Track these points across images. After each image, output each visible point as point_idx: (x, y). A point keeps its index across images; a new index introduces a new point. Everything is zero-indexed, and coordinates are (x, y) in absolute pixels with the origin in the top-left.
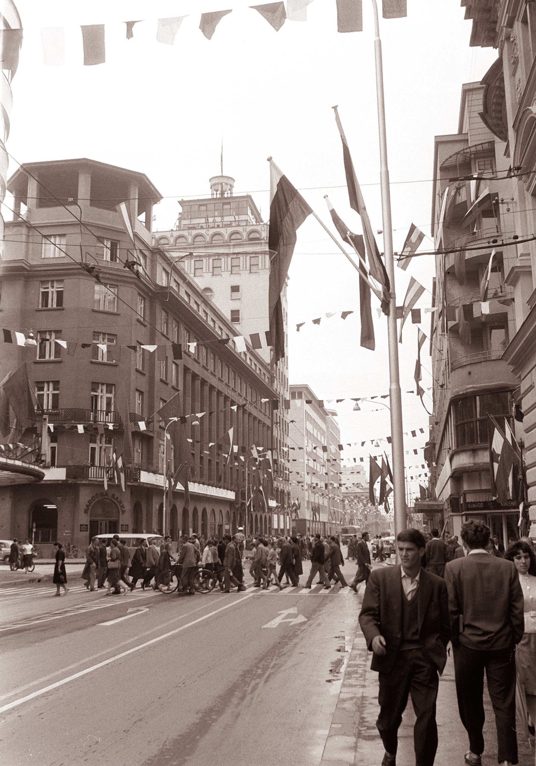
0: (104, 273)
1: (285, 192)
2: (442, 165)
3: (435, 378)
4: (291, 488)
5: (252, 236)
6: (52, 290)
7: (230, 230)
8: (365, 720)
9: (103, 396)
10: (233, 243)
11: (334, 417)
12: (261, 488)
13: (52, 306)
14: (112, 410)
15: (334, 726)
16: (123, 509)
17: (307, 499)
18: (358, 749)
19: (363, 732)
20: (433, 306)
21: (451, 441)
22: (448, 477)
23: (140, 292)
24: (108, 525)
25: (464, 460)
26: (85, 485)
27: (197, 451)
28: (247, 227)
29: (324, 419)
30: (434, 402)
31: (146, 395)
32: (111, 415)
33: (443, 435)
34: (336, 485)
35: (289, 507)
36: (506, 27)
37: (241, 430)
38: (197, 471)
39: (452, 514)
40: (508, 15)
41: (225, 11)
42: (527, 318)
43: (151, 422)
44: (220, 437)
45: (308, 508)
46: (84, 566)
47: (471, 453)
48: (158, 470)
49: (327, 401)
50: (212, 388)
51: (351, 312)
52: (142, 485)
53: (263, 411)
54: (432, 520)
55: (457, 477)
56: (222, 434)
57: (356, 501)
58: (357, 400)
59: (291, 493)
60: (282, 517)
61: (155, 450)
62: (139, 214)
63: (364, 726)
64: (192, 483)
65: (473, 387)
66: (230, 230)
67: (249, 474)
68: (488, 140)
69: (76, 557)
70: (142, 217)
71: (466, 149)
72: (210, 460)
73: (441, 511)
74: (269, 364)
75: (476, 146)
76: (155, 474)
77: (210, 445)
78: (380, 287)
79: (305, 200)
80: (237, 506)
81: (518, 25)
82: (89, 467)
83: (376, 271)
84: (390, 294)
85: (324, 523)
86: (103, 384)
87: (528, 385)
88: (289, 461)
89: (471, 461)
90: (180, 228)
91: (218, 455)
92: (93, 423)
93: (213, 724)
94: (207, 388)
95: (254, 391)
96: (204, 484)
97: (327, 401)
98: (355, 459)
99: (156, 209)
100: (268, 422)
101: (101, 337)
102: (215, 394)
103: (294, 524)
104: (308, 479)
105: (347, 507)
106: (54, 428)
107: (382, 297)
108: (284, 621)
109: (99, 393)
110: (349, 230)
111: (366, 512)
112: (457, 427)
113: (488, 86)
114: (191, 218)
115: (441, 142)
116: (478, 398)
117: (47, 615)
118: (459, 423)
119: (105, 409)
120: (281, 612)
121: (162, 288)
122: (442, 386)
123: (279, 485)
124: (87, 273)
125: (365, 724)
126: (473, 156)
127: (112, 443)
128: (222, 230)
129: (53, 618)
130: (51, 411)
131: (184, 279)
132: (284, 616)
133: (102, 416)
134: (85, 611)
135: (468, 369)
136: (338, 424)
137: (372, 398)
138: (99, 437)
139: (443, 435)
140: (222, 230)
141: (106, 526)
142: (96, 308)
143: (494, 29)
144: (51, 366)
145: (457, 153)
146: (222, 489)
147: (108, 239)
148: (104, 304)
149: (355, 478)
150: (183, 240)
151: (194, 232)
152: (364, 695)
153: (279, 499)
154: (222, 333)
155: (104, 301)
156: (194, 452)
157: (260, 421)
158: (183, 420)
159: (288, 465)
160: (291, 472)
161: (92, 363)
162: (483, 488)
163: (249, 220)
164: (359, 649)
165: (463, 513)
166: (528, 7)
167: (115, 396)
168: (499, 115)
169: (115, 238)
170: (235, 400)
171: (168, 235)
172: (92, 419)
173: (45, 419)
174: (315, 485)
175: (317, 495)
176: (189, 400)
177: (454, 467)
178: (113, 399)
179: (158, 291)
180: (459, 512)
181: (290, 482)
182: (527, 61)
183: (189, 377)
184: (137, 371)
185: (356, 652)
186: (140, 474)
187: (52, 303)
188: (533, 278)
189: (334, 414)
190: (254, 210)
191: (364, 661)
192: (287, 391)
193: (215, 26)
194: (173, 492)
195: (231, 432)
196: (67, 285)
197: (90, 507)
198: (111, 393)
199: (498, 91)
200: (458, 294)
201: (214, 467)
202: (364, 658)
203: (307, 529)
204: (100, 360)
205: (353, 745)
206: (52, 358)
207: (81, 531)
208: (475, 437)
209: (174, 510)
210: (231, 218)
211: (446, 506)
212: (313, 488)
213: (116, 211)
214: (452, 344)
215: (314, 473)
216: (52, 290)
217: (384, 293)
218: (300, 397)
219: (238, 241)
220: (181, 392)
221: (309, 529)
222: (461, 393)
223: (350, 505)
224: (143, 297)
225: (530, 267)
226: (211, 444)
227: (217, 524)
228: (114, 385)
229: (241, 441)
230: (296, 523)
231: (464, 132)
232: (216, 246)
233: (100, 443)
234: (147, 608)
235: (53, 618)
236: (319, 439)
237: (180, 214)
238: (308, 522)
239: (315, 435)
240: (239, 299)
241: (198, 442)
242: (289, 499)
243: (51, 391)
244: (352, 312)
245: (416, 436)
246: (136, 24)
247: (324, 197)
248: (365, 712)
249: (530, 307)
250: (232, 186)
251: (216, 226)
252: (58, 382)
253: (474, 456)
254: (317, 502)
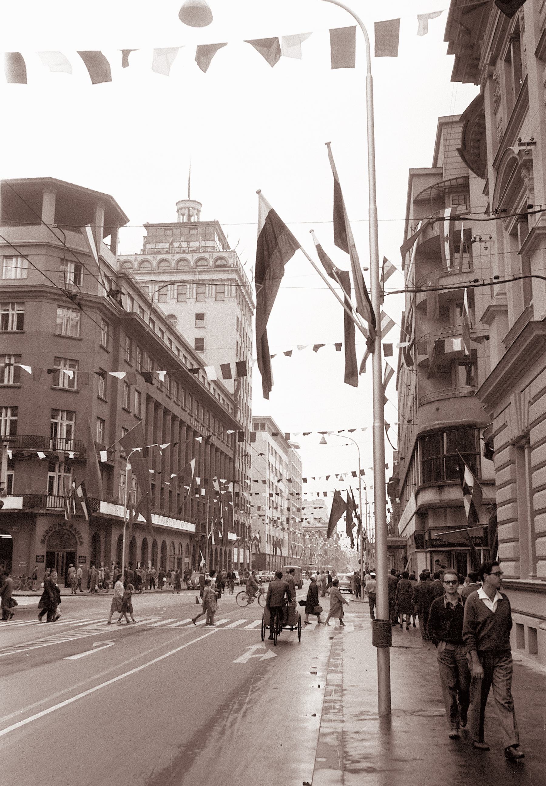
0: (86, 300)
1: (274, 225)
2: (416, 198)
3: (401, 413)
4: (252, 521)
5: (218, 263)
6: (13, 313)
7: (196, 256)
8: (349, 754)
9: (63, 423)
10: (199, 269)
11: (296, 449)
12: (222, 521)
13: (12, 329)
14: (73, 438)
15: (319, 759)
16: (81, 540)
17: (267, 532)
18: (345, 782)
19: (348, 765)
21: (416, 476)
22: (413, 513)
23: (104, 317)
24: (65, 556)
25: (429, 496)
26: (41, 515)
27: (158, 483)
28: (214, 254)
29: (286, 452)
30: (399, 436)
31: (107, 424)
32: (71, 443)
33: (409, 470)
34: (298, 520)
35: (249, 540)
36: (489, 65)
37: (202, 460)
38: (158, 502)
39: (416, 550)
40: (491, 53)
41: (220, 44)
42: (504, 357)
43: (113, 452)
44: (182, 468)
45: (268, 542)
46: (40, 598)
47: (437, 489)
48: (118, 501)
49: (294, 434)
50: (174, 417)
51: (322, 345)
52: (101, 515)
54: (394, 556)
55: (422, 513)
56: (183, 466)
57: (317, 535)
58: (323, 433)
59: (252, 526)
60: (242, 551)
61: (115, 480)
62: (105, 236)
63: (349, 760)
64: (157, 516)
65: (441, 424)
66: (196, 256)
67: (209, 506)
68: (462, 176)
69: (31, 588)
70: (108, 240)
71: (441, 183)
72: (171, 492)
73: (404, 547)
74: (232, 395)
75: (450, 180)
76: (115, 504)
77: (172, 477)
78: (366, 324)
79: (294, 235)
80: (197, 539)
81: (501, 64)
82: (46, 496)
83: (364, 309)
84: (375, 332)
85: (285, 557)
86: (63, 411)
87: (501, 424)
88: (251, 494)
89: (437, 497)
90: (144, 252)
91: (180, 486)
92: (52, 450)
93: (196, 758)
94: (169, 418)
95: (217, 423)
96: (164, 515)
97: (294, 434)
98: (318, 494)
99: (122, 232)
100: (230, 454)
101: (62, 362)
102: (177, 424)
103: (254, 558)
104: (269, 513)
105: (308, 541)
106: (13, 455)
107: (368, 334)
108: (253, 656)
109: (58, 420)
110: (334, 266)
111: (326, 547)
112: (423, 463)
113: (468, 122)
114: (156, 243)
115: (415, 175)
116: (445, 434)
117: (10, 648)
118: (426, 459)
119: (65, 437)
120: (250, 647)
121: (127, 314)
122: (409, 422)
123: (239, 518)
124: (68, 299)
125: (348, 758)
126: (447, 190)
127: (72, 472)
128: (188, 256)
129: (17, 651)
130: (8, 437)
131: (149, 305)
132: (252, 651)
133: (61, 444)
134: (50, 644)
135: (436, 405)
136: (300, 457)
137: (339, 432)
138: (57, 466)
139: (409, 470)
140: (188, 256)
141: (63, 557)
142: (58, 333)
143: (477, 66)
144: (9, 391)
145: (431, 187)
146: (182, 522)
147: (72, 262)
148: (67, 328)
149: (318, 513)
150: (148, 265)
151: (159, 257)
152: (344, 730)
153: (240, 533)
154: (186, 362)
155: (67, 325)
156: (154, 483)
157: (222, 452)
158: (146, 451)
159: (249, 498)
160: (252, 506)
161: (52, 389)
162: (449, 525)
163: (216, 246)
164: (333, 685)
165: (428, 550)
166: (512, 46)
167: (75, 423)
168: (477, 152)
169: (80, 261)
170: (198, 431)
171: (132, 259)
172: (51, 447)
173: (6, 446)
174: (276, 519)
175: (278, 529)
176: (151, 429)
177: (419, 504)
178: (73, 427)
179: (122, 317)
180: (423, 548)
181: (251, 515)
182: (509, 101)
183: (152, 406)
184: (99, 398)
185: (330, 688)
186: (99, 504)
187: (13, 326)
188: (509, 317)
189: (297, 447)
190: (221, 236)
191: (340, 696)
192: (250, 422)
193: (210, 60)
194: (134, 524)
195: (193, 463)
196: (28, 308)
197: (47, 538)
198: (71, 420)
199: (476, 128)
200: (428, 331)
201: (175, 498)
202: (339, 694)
203: (267, 563)
204: (61, 386)
205: (340, 778)
206: (11, 383)
207: (37, 562)
208: (442, 473)
209: (132, 543)
210: (196, 244)
211: (410, 542)
212: (274, 522)
213: (81, 233)
214: (421, 379)
215: (276, 508)
216: (13, 312)
217: (370, 330)
218: (263, 428)
219: (204, 267)
220: (143, 422)
221: (269, 563)
222: (428, 429)
223: (310, 540)
224: (106, 322)
225: (506, 306)
226: (173, 476)
227: (176, 557)
228: (75, 412)
229: (202, 473)
230: (256, 557)
231: (438, 166)
233: (59, 472)
234: (112, 641)
235: (17, 651)
236: (281, 472)
237: (145, 237)
238: (268, 556)
239: (277, 468)
240: (204, 327)
241: (159, 473)
242: (250, 532)
243: (9, 417)
244: (324, 345)
246: (131, 52)
247: (310, 232)
248: (347, 746)
249: (505, 346)
250: (199, 211)
251: (182, 252)
252: (16, 408)
253: (440, 494)
254: (277, 536)
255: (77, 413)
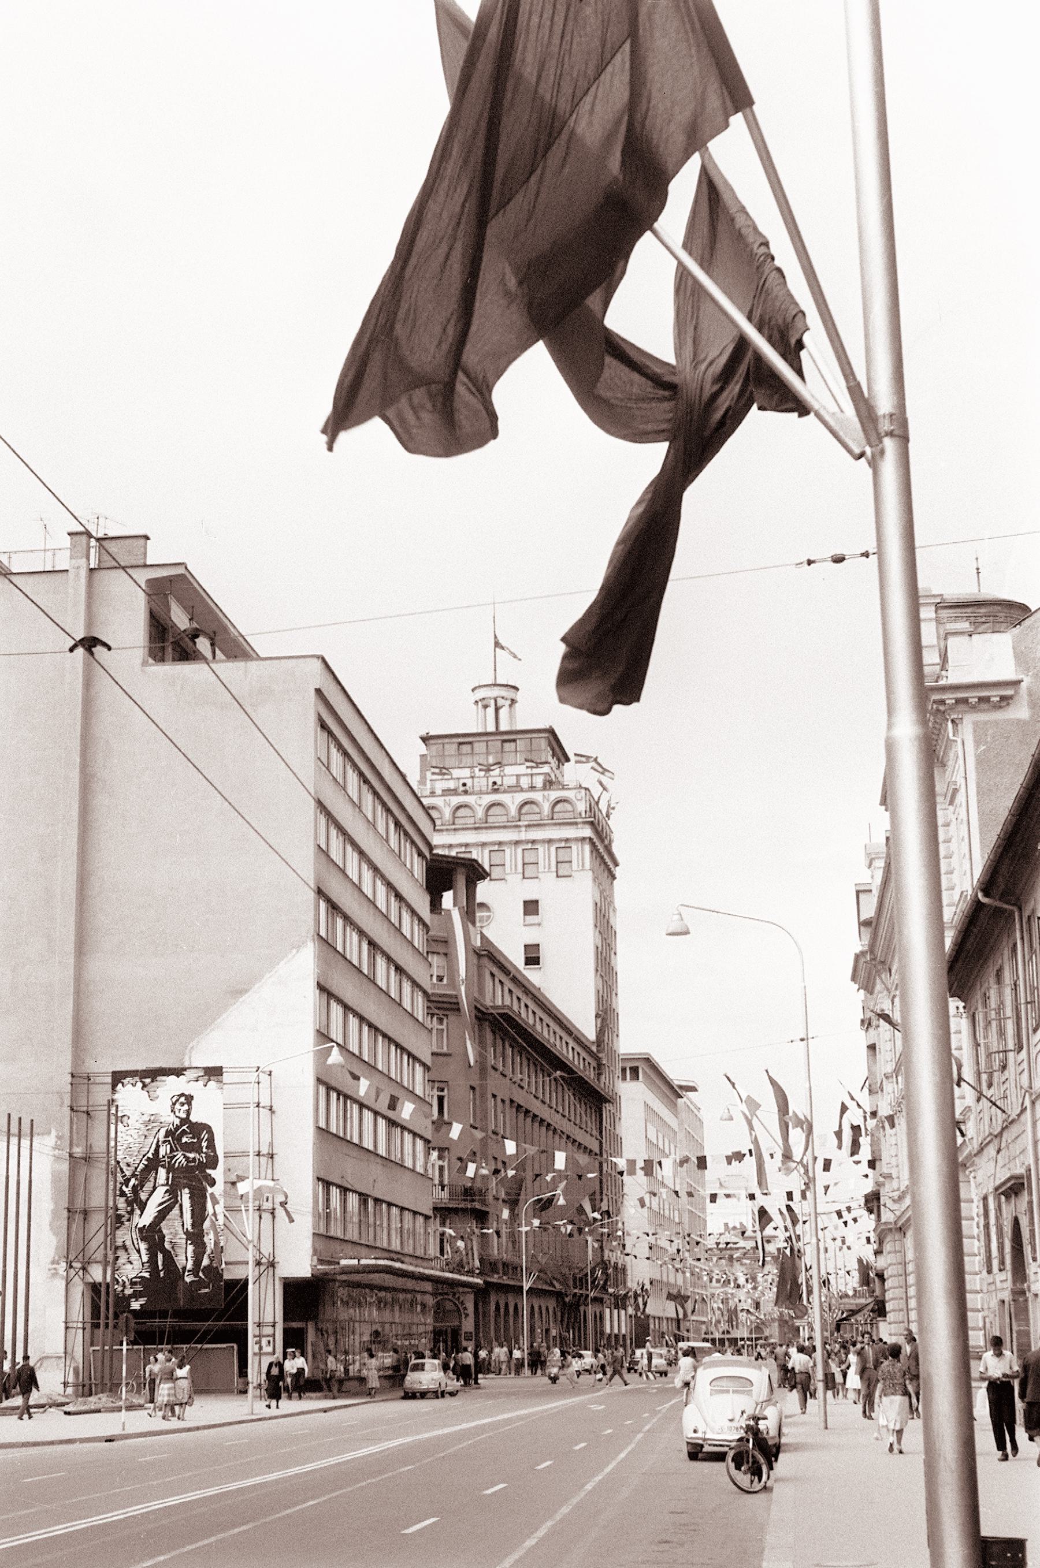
20: (728, 1392)
29: (673, 1107)
53: (578, 1122)
228: (447, 1149)
232: (495, 827)
238: (651, 1321)
245: (825, 1160)
250: (513, 701)
255: (451, 1149)
